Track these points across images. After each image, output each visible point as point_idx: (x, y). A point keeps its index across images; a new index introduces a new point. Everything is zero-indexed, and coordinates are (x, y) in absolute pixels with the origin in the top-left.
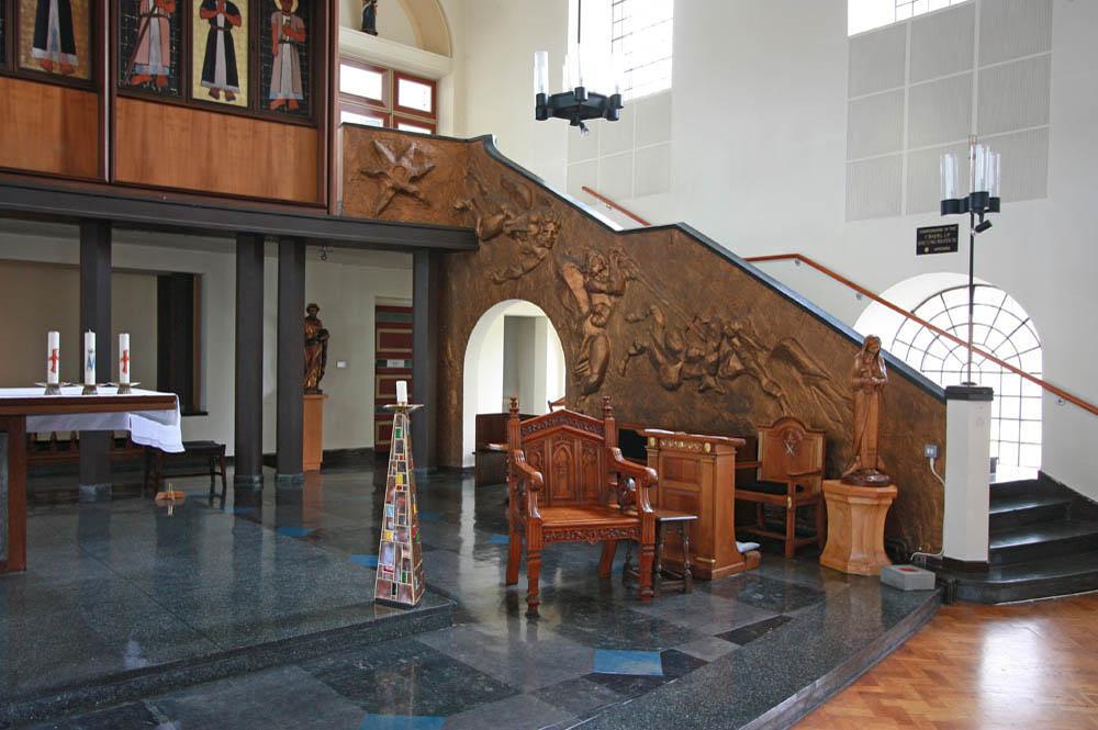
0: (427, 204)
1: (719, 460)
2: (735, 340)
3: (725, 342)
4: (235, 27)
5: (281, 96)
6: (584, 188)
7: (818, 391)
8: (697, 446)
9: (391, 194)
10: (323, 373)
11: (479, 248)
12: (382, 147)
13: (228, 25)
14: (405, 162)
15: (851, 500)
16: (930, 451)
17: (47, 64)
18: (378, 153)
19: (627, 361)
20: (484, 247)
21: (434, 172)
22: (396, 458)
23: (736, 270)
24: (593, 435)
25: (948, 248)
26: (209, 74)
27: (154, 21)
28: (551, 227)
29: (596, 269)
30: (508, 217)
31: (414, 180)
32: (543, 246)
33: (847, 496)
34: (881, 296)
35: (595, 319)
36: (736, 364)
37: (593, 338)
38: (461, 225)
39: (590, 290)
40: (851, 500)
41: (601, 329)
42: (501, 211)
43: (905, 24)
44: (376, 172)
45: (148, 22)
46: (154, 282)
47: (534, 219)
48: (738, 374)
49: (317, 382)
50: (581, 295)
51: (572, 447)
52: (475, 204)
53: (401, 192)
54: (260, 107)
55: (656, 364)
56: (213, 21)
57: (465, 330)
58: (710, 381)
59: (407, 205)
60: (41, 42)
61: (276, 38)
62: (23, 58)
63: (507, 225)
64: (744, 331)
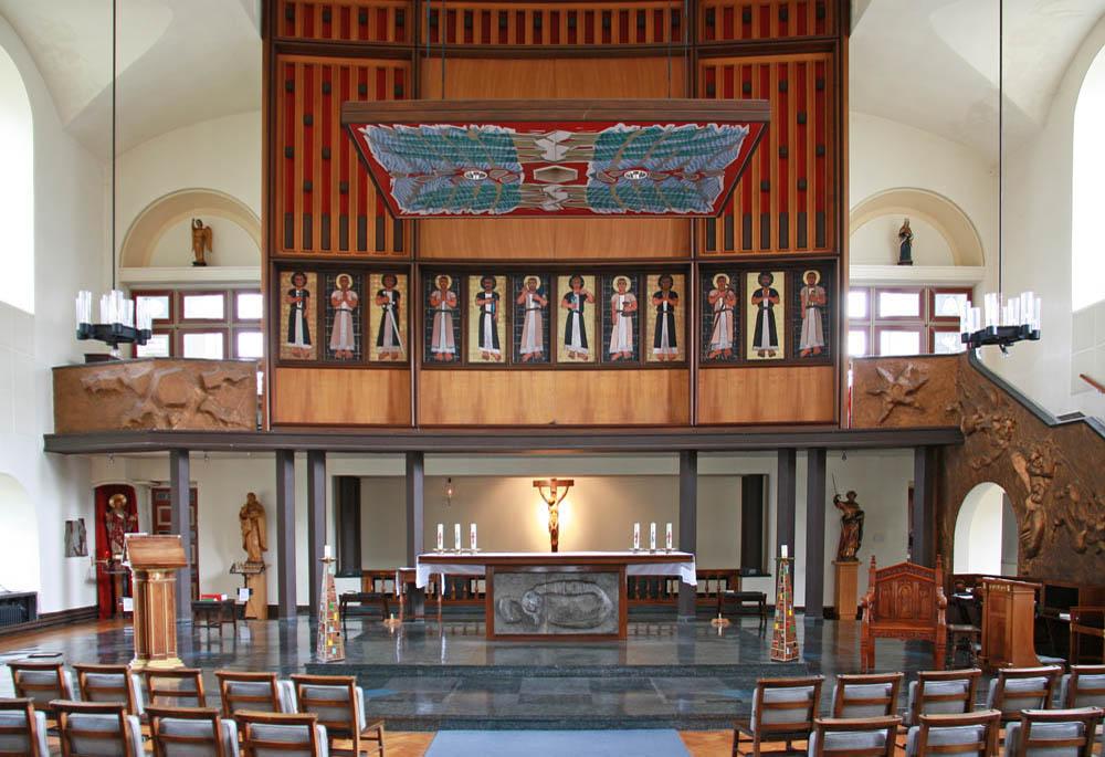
0: (922, 410)
1: (1015, 597)
4: (775, 305)
5: (808, 346)
6: (1082, 376)
9: (890, 406)
10: (859, 545)
11: (963, 443)
12: (883, 372)
13: (771, 304)
14: (902, 381)
17: (660, 356)
18: (880, 376)
19: (1055, 531)
20: (968, 441)
21: (928, 384)
26: (758, 342)
27: (723, 314)
29: (1033, 457)
30: (981, 417)
31: (910, 393)
38: (953, 424)
41: (1039, 506)
42: (976, 412)
45: (719, 316)
46: (740, 480)
49: (855, 552)
50: (1026, 477)
51: (912, 587)
52: (962, 407)
53: (897, 403)
54: (794, 358)
55: (1070, 532)
56: (760, 305)
59: (905, 412)
60: (658, 345)
61: (804, 305)
62: (648, 355)
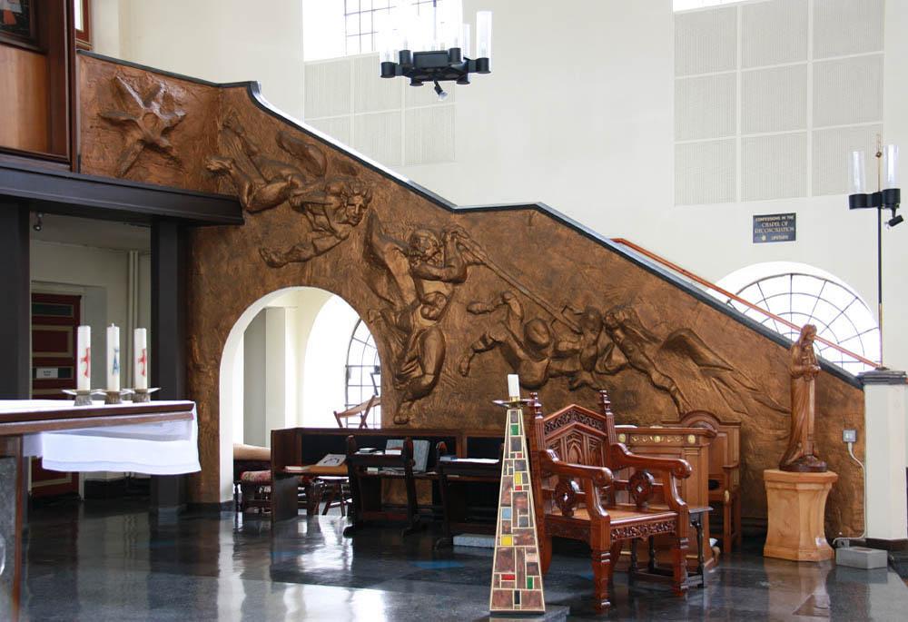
2: (618, 332)
3: (603, 334)
7: (717, 382)
8: (678, 439)
15: (800, 487)
16: (849, 435)
21: (185, 122)
22: (513, 456)
23: (616, 257)
24: (596, 430)
25: (787, 237)
28: (358, 200)
29: (429, 252)
30: (293, 186)
31: (166, 132)
32: (346, 222)
33: (795, 483)
34: (716, 285)
35: (426, 311)
36: (618, 358)
37: (424, 334)
39: (418, 276)
40: (800, 487)
43: (736, 7)
44: (123, 118)
47: (335, 188)
48: (621, 368)
50: (407, 283)
57: (223, 324)
58: (586, 377)
63: (296, 196)
64: (630, 321)
